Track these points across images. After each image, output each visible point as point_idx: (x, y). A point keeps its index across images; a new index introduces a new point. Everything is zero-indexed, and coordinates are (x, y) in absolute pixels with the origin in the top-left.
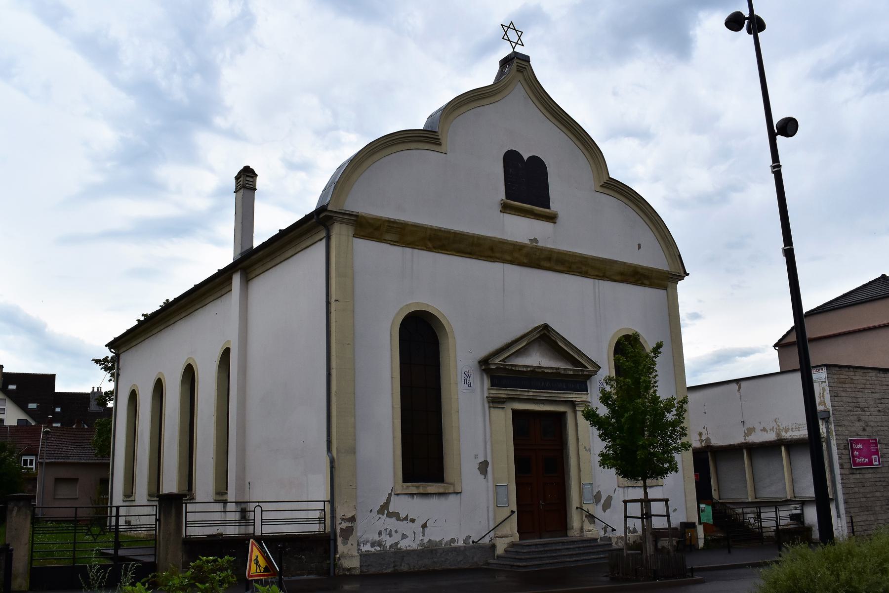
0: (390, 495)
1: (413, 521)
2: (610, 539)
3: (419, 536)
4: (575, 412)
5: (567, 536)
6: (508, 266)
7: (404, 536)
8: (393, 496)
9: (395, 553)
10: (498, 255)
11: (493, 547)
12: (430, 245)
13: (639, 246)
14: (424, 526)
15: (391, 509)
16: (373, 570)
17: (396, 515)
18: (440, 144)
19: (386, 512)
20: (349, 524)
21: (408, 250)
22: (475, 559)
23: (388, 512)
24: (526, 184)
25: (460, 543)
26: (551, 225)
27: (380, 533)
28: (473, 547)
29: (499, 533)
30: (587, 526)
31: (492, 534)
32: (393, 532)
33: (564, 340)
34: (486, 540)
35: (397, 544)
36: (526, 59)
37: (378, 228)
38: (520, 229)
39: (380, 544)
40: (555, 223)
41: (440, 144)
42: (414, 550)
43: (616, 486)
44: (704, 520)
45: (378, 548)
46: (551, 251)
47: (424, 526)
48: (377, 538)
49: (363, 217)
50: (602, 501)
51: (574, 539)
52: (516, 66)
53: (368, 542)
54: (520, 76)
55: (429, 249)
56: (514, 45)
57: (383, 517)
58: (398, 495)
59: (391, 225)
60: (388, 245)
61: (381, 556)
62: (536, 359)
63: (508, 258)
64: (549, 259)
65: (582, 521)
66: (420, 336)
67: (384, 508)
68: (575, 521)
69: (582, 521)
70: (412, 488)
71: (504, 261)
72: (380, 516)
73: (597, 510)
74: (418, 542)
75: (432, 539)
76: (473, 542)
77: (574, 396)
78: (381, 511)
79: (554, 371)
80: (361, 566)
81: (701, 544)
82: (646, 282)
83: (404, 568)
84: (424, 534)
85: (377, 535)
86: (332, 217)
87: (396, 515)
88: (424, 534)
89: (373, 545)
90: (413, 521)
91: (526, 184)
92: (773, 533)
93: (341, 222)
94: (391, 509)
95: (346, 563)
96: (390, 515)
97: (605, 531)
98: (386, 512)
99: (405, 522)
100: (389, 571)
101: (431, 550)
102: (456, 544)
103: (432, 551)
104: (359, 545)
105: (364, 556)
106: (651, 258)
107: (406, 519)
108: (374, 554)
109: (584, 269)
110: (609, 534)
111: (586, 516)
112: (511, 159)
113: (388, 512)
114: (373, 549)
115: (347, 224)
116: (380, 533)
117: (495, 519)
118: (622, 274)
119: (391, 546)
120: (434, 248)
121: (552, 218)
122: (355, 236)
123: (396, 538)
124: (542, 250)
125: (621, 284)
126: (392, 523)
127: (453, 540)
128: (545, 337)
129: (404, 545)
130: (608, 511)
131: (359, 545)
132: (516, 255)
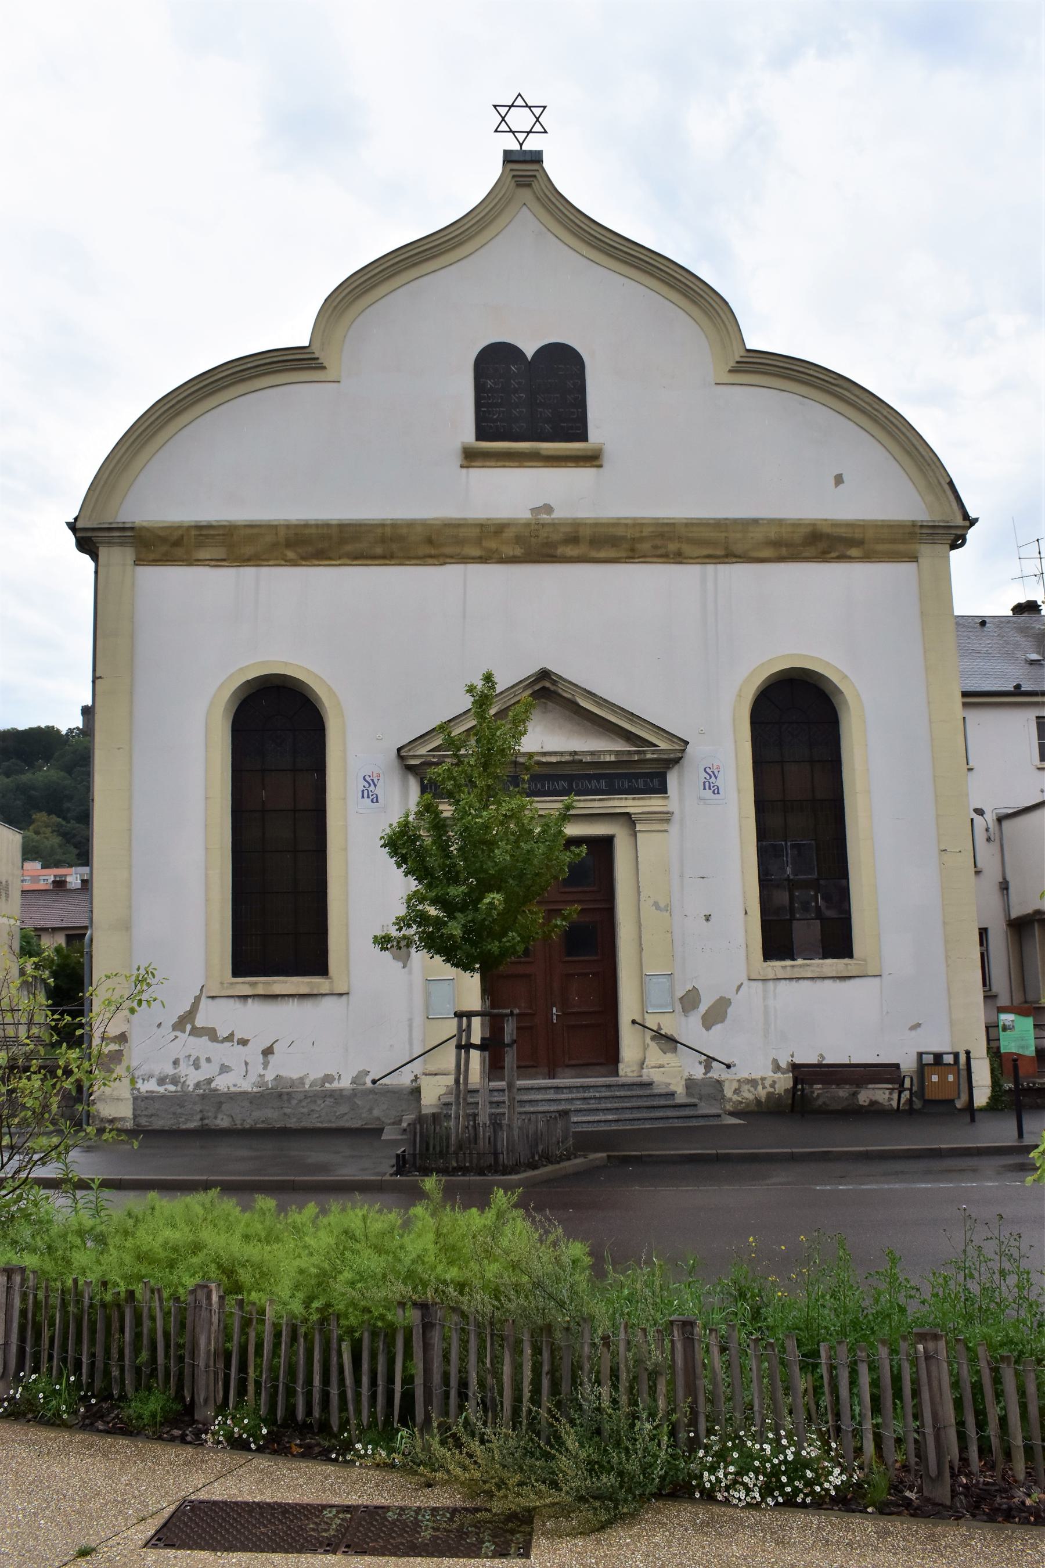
0: (197, 999)
1: (244, 1042)
2: (719, 1083)
3: (256, 1068)
4: (634, 834)
5: (617, 1075)
6: (475, 570)
7: (224, 1069)
8: (203, 1000)
9: (203, 1097)
10: (448, 550)
11: (416, 1092)
12: (290, 554)
13: (839, 480)
14: (268, 1052)
15: (199, 1022)
16: (158, 1124)
17: (211, 1034)
18: (322, 368)
19: (189, 1027)
20: (116, 1047)
21: (249, 572)
22: (376, 1113)
23: (194, 1028)
24: (530, 399)
25: (345, 1083)
26: (592, 471)
27: (176, 1063)
28: (371, 1091)
29: (432, 1068)
30: (655, 1054)
31: (417, 1067)
32: (203, 1062)
33: (590, 695)
34: (404, 1079)
35: (209, 1081)
36: (536, 157)
37: (178, 543)
38: (513, 492)
39: (175, 1081)
40: (601, 466)
41: (322, 368)
42: (245, 1093)
43: (743, 978)
44: (1008, 1045)
45: (172, 1088)
46: (577, 524)
47: (268, 1052)
48: (170, 1070)
49: (142, 529)
50: (703, 1008)
51: (629, 1080)
52: (523, 168)
53: (151, 1076)
54: (525, 194)
55: (294, 563)
56: (521, 137)
57: (183, 1037)
58: (213, 997)
59: (204, 532)
60: (207, 569)
61: (179, 1100)
62: (543, 738)
63: (476, 552)
64: (573, 539)
65: (645, 1048)
66: (277, 731)
67: (185, 1021)
68: (631, 1046)
69: (645, 1048)
70: (244, 985)
71: (465, 560)
72: (178, 1033)
73: (688, 1028)
74: (253, 1078)
75: (284, 1073)
76: (374, 1082)
77: (630, 803)
78: (180, 1025)
79: (567, 758)
80: (135, 1117)
81: (982, 1097)
82: (854, 552)
83: (223, 1122)
84: (266, 1065)
85: (171, 1066)
86: (90, 538)
87: (211, 1034)
88: (266, 1065)
89: (161, 1081)
90: (244, 1042)
91: (530, 399)
92: (487, 1054)
93: (110, 544)
94: (199, 1022)
95: (105, 1110)
96: (196, 1032)
97: (708, 1068)
98: (189, 1027)
99: (227, 1044)
100: (191, 1125)
101: (279, 1094)
102: (336, 1085)
103: (280, 1095)
104: (133, 1081)
105: (140, 1101)
106: (880, 497)
107: (230, 1038)
108: (163, 1097)
109: (672, 547)
110: (718, 1072)
111: (653, 1038)
112: (495, 363)
113: (194, 1028)
114: (161, 1090)
115: (121, 545)
116: (176, 1063)
117: (424, 1041)
118: (776, 544)
119: (198, 1085)
120: (303, 558)
121: (592, 459)
122: (139, 562)
123: (206, 1071)
124: (554, 525)
125: (781, 566)
126: (201, 1046)
127: (328, 1078)
128: (546, 690)
129: (223, 1083)
130: (717, 1028)
131: (133, 1081)
132: (492, 544)
